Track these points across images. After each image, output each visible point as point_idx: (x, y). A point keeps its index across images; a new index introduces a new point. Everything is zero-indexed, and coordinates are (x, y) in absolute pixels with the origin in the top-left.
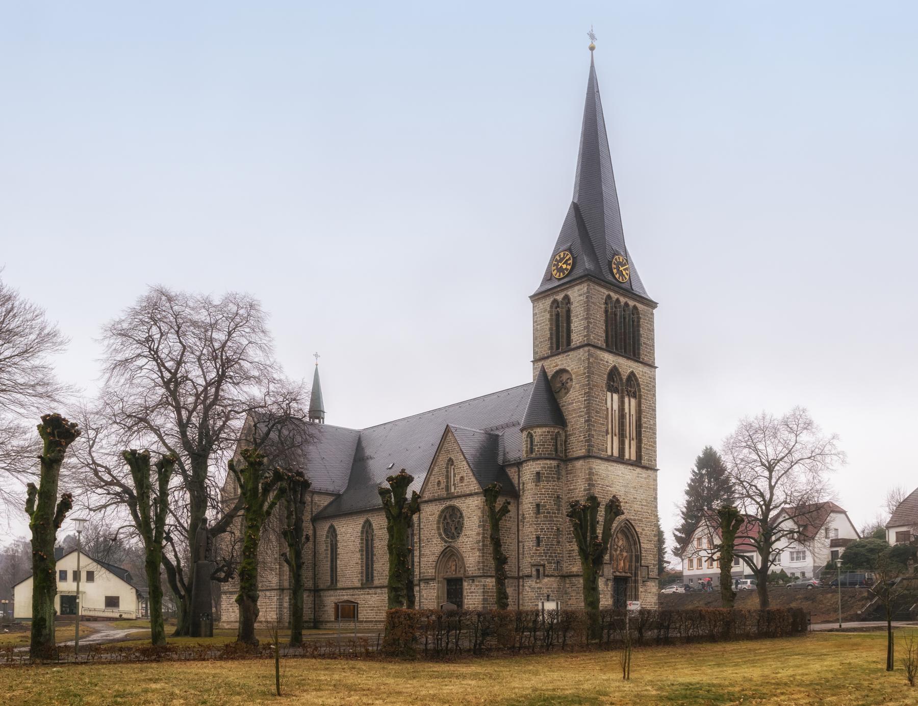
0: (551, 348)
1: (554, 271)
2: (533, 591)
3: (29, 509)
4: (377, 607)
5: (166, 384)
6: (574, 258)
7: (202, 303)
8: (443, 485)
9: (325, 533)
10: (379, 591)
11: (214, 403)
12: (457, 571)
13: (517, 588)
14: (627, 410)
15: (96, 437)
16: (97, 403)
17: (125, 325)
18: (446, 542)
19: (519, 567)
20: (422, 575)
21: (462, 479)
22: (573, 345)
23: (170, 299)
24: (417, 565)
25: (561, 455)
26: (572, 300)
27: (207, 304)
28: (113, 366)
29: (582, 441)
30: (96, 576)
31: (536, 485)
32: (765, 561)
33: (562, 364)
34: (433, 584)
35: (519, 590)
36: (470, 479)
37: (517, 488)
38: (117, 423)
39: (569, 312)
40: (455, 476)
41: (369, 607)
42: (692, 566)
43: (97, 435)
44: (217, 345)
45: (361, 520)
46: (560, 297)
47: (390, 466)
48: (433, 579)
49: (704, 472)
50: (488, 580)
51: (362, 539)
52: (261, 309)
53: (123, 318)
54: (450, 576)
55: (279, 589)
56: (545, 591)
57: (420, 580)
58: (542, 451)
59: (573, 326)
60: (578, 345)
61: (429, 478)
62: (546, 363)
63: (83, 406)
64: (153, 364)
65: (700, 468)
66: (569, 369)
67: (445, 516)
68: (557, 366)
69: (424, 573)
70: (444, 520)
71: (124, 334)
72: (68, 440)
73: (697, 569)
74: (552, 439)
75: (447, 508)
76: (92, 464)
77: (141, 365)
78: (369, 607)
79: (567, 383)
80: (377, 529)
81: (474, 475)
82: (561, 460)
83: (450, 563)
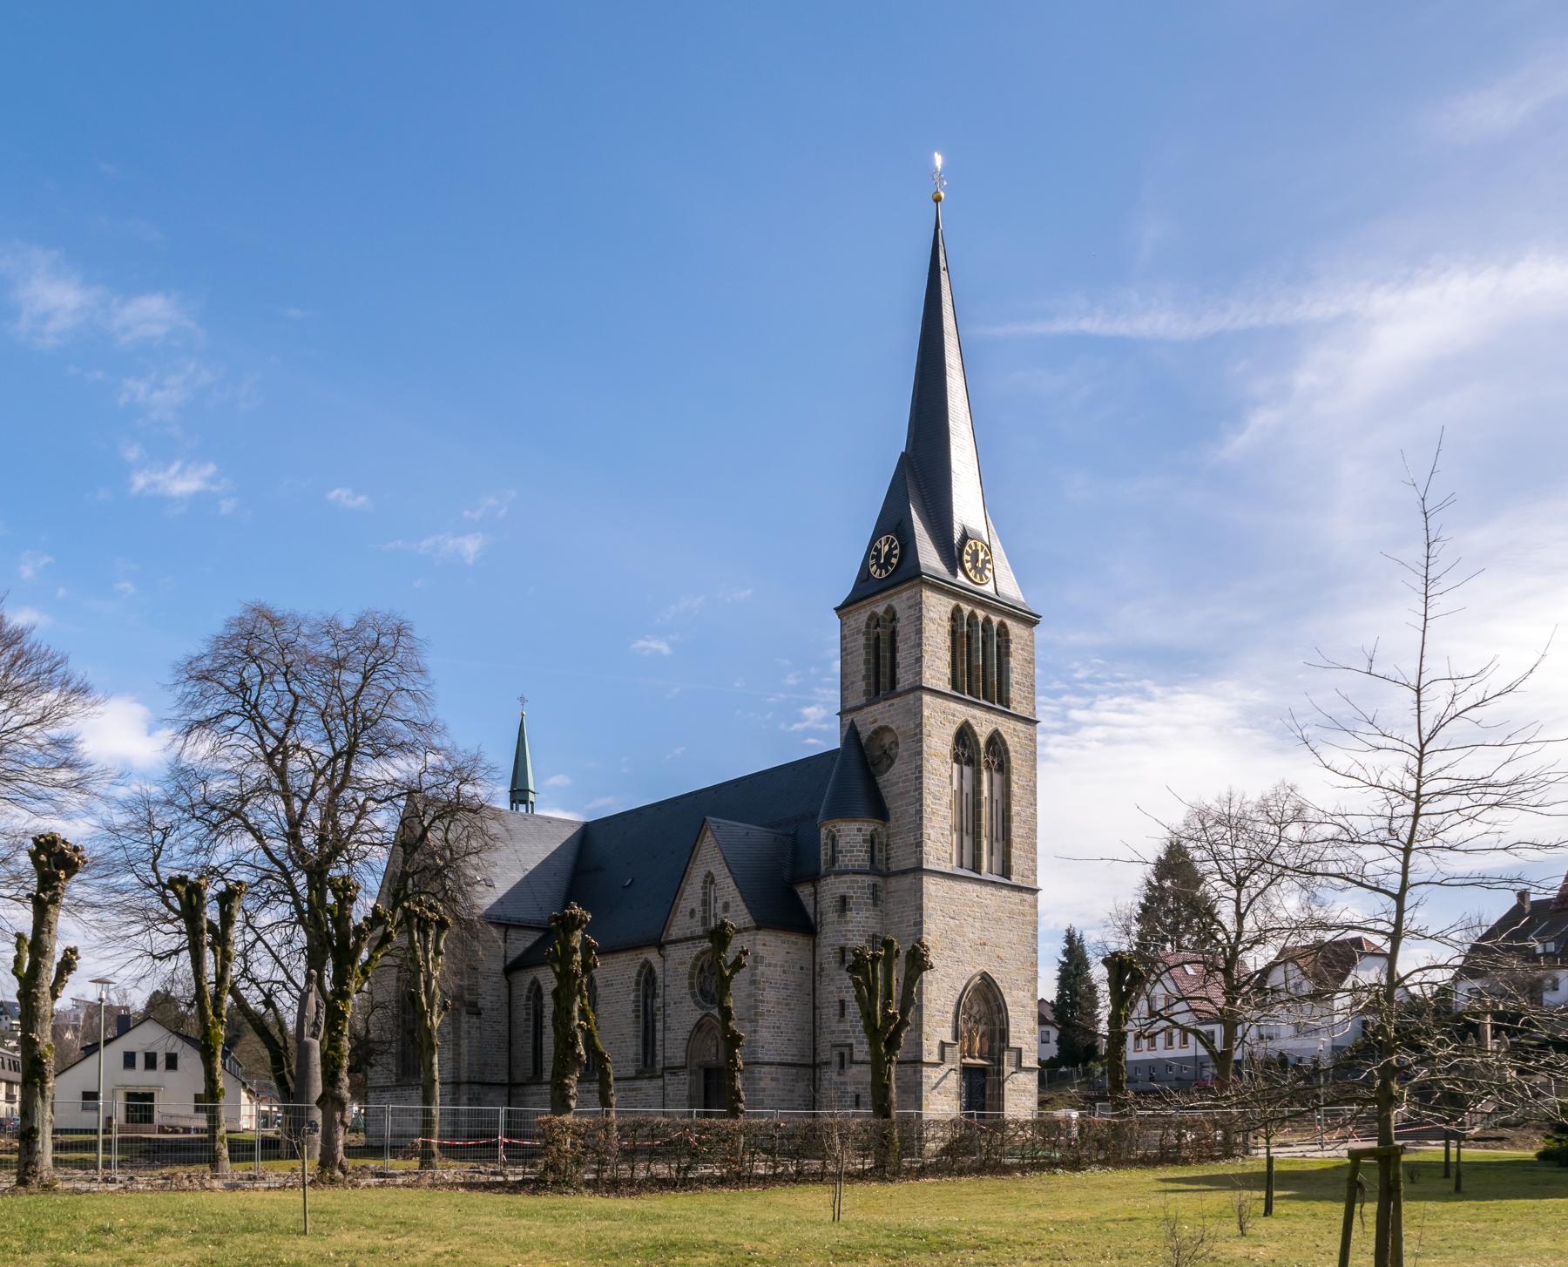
0: (867, 693)
1: (872, 566)
3: (16, 971)
5: (270, 757)
7: (325, 626)
8: (698, 916)
11: (342, 786)
14: (986, 793)
15: (163, 842)
16: (166, 786)
17: (207, 663)
18: (702, 1008)
19: (815, 1049)
21: (726, 907)
22: (899, 687)
23: (274, 622)
25: (880, 867)
26: (898, 615)
27: (330, 628)
28: (187, 729)
29: (912, 844)
30: (180, 1063)
31: (839, 916)
32: (1229, 1037)
33: (883, 719)
34: (684, 1077)
36: (738, 906)
37: (813, 921)
38: (198, 819)
39: (894, 633)
40: (716, 902)
42: (1171, 1043)
43: (164, 838)
44: (348, 692)
47: (627, 883)
49: (1168, 884)
52: (414, 634)
53: (205, 652)
55: (453, 1083)
56: (851, 1088)
57: (664, 1069)
59: (899, 657)
60: (907, 687)
62: (858, 717)
63: (145, 795)
64: (248, 726)
65: (1160, 877)
66: (893, 726)
68: (875, 721)
69: (670, 1058)
70: (700, 973)
71: (204, 677)
72: (70, 871)
73: (1180, 1047)
74: (864, 841)
76: (157, 885)
77: (232, 726)
79: (891, 749)
81: (744, 900)
82: (879, 873)
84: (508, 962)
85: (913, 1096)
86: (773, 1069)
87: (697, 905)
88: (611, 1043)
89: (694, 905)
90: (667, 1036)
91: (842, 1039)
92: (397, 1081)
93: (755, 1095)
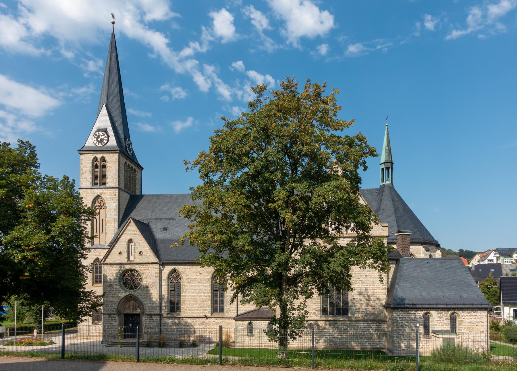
8: (125, 255)
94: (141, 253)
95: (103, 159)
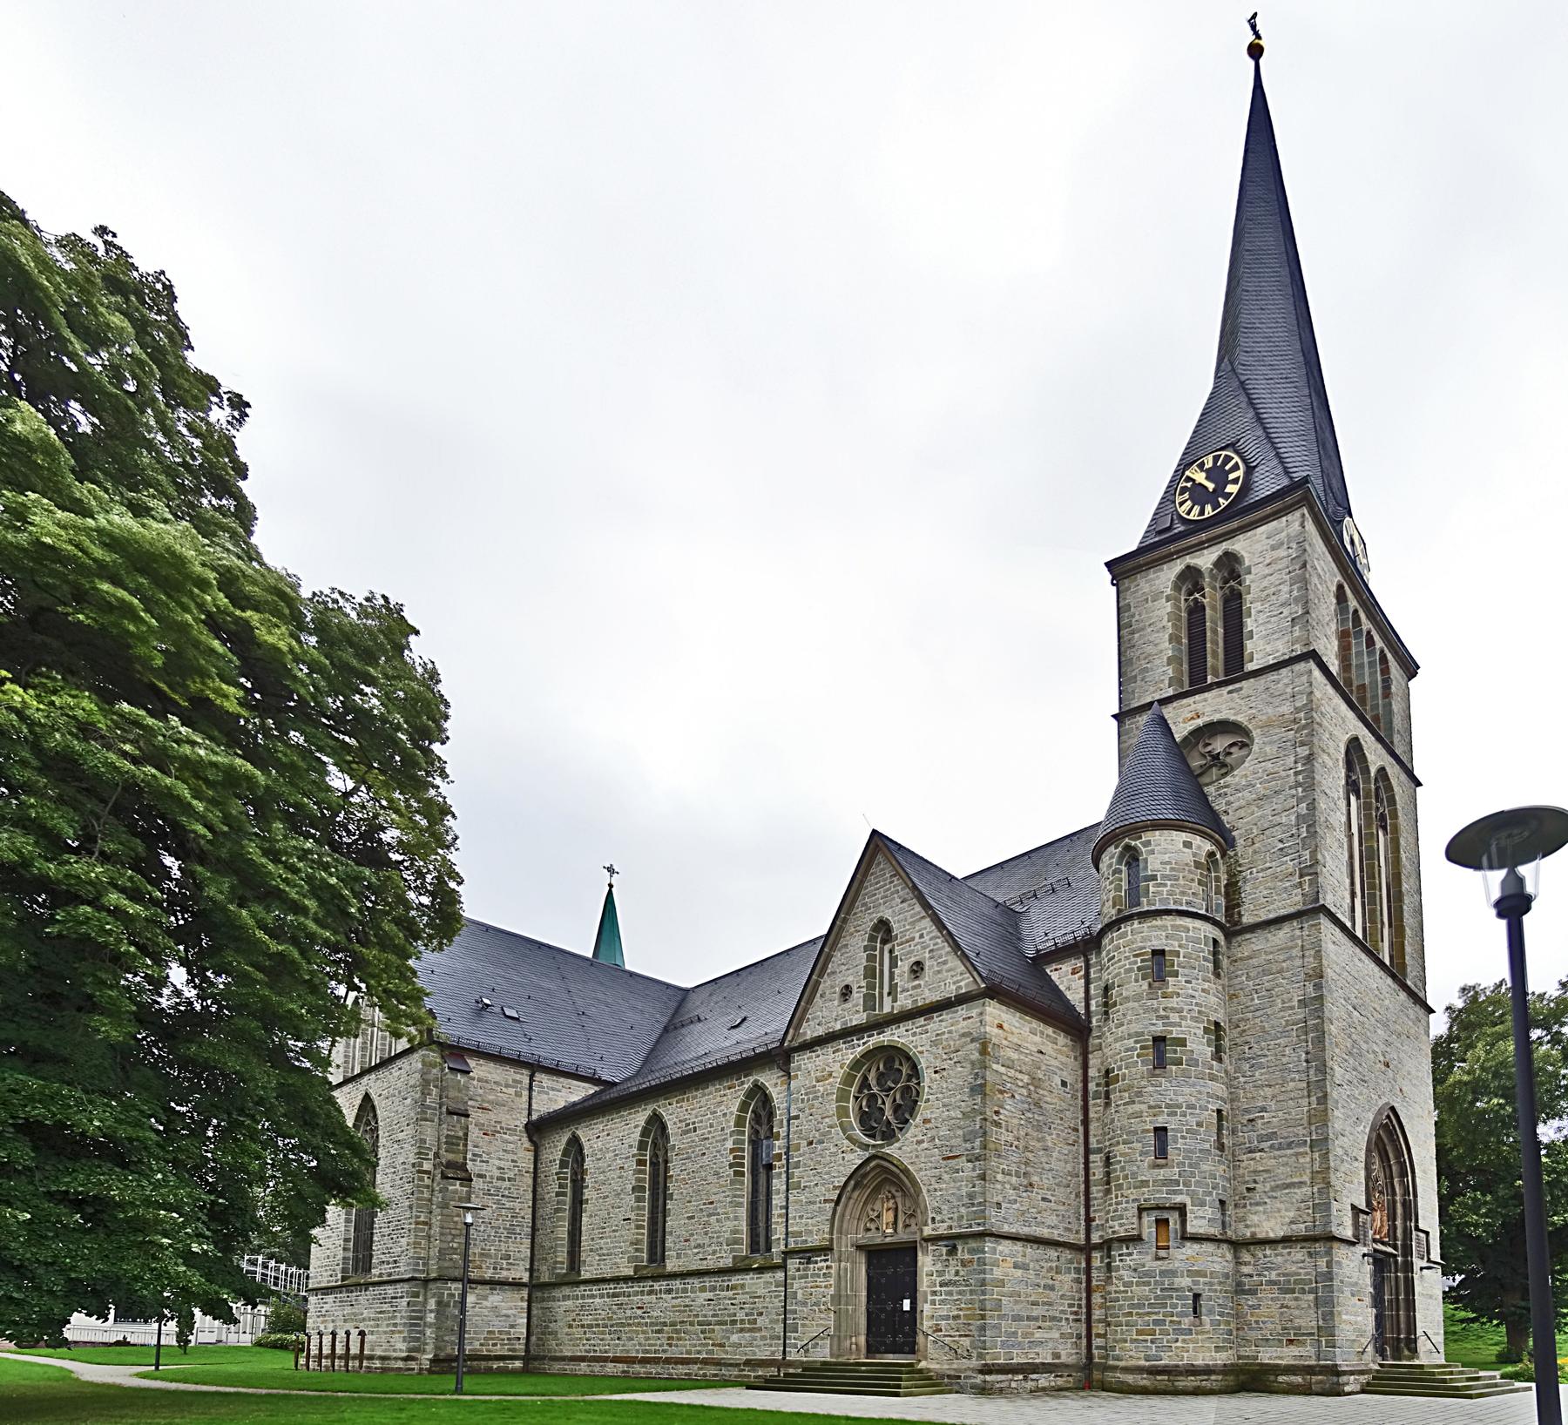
2: (1149, 1284)
4: (673, 1324)
6: (1250, 470)
8: (857, 997)
9: (558, 1155)
10: (677, 1284)
12: (900, 1225)
13: (1084, 1278)
18: (866, 1147)
20: (791, 1240)
21: (917, 969)
24: (780, 1216)
35: (1089, 1281)
36: (945, 963)
40: (893, 964)
41: (652, 1324)
45: (640, 1117)
46: (1205, 560)
48: (826, 1250)
50: (1000, 1248)
51: (641, 1163)
54: (878, 1241)
57: (787, 1254)
58: (1171, 893)
61: (818, 983)
67: (865, 1078)
69: (800, 1234)
75: (868, 1055)
78: (652, 1324)
80: (676, 1134)
83: (878, 1206)
84: (535, 1117)
85: (1311, 1297)
86: (1018, 1247)
87: (856, 979)
88: (692, 1217)
89: (849, 980)
90: (791, 1198)
91: (1162, 1196)
92: (343, 1279)
93: (984, 1293)
94: (917, 969)
95: (1230, 566)
